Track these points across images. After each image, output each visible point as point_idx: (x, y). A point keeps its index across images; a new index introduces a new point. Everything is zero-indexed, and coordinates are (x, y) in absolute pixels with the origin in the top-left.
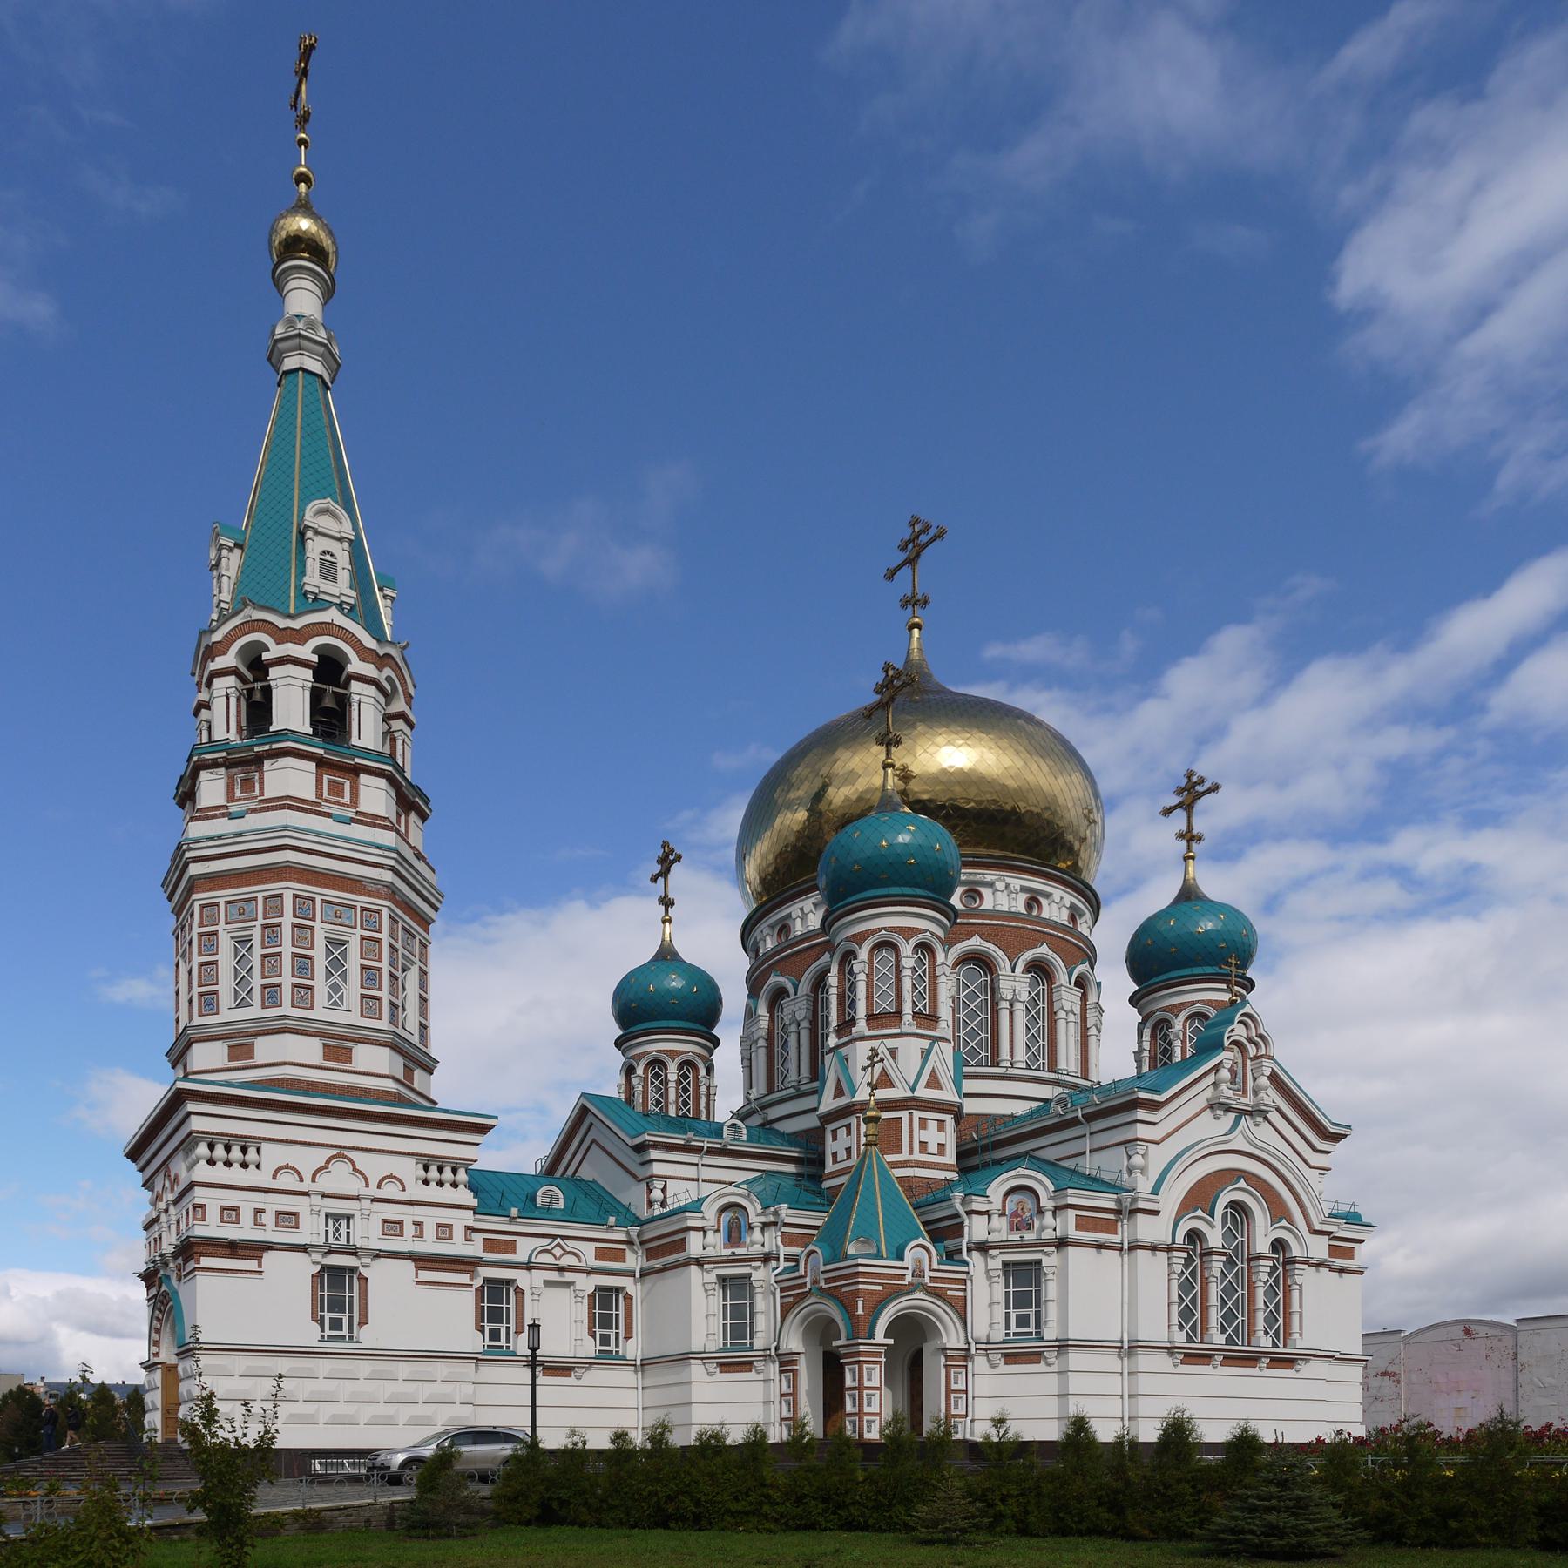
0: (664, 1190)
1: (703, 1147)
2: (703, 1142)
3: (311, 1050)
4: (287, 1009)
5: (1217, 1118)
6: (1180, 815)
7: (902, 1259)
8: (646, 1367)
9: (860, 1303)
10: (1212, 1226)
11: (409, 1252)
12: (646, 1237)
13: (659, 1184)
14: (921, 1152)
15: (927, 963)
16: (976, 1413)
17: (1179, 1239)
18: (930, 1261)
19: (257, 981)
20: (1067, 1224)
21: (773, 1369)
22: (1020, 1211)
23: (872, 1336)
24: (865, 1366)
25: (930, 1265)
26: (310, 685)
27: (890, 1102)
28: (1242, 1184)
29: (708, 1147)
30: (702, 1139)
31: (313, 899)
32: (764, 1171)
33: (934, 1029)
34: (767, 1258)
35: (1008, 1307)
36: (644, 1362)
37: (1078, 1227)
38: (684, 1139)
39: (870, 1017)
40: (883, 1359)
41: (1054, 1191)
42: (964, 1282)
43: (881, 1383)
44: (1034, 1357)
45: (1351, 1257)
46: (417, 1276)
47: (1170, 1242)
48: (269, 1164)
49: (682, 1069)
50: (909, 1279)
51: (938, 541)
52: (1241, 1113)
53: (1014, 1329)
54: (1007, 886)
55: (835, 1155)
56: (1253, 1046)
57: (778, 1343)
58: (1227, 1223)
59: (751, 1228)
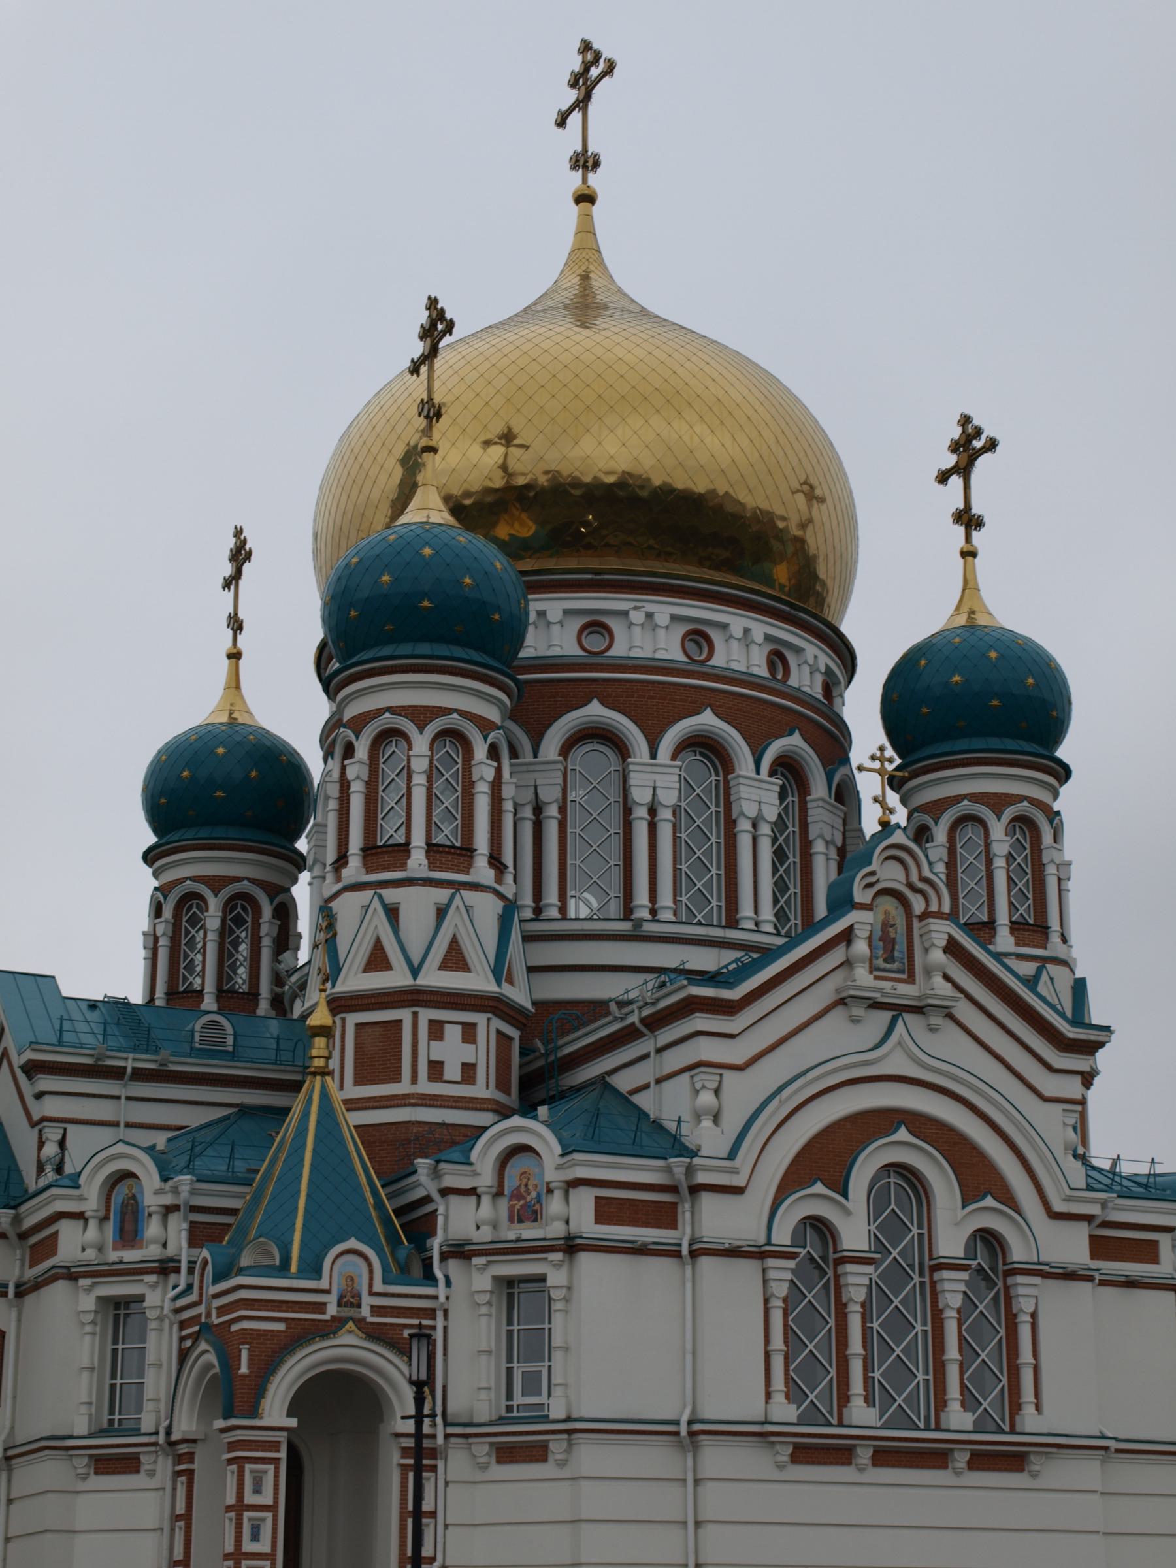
1: (125, 1068)
2: (126, 1059)
5: (855, 1021)
6: (956, 481)
8: (14, 1461)
9: (244, 1355)
10: (847, 1212)
12: (28, 1223)
13: (53, 1134)
17: (782, 1236)
18: (371, 1279)
20: (584, 1221)
21: (164, 1466)
22: (523, 1189)
23: (254, 1412)
24: (248, 1467)
25: (371, 1286)
28: (903, 1134)
29: (134, 1069)
30: (124, 1055)
33: (466, 870)
34: (166, 1268)
35: (510, 1359)
36: (10, 1453)
37: (600, 1218)
38: (92, 1056)
42: (431, 1313)
44: (536, 1453)
47: (762, 1240)
49: (234, 907)
50: (332, 1310)
51: (606, 79)
52: (899, 1009)
53: (519, 1399)
57: (171, 1421)
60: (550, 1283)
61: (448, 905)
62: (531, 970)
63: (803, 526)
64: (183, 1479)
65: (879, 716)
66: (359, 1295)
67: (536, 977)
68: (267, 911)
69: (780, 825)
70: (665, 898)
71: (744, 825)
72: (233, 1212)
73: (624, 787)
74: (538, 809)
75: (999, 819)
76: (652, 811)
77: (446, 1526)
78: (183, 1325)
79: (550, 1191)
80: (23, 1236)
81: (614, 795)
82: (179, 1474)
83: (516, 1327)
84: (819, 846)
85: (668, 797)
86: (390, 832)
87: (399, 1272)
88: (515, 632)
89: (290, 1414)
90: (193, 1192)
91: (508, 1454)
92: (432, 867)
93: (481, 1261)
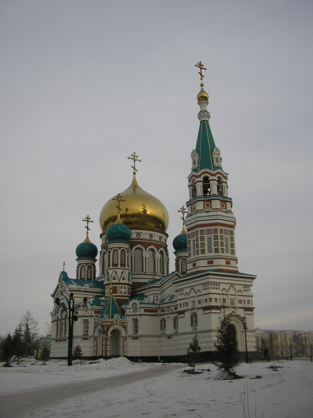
3: (223, 262)
4: (200, 255)
7: (113, 318)
9: (105, 328)
11: (243, 307)
14: (121, 293)
18: (119, 319)
19: (213, 247)
25: (119, 319)
26: (217, 184)
31: (222, 230)
35: (85, 329)
39: (113, 264)
40: (110, 339)
42: (126, 323)
43: (109, 344)
46: (245, 312)
48: (221, 288)
55: (106, 293)
59: (89, 310)
62: (132, 278)
63: (163, 219)
64: (96, 341)
65: (173, 246)
67: (132, 279)
69: (160, 260)
70: (147, 269)
71: (156, 260)
72: (101, 310)
74: (132, 258)
76: (146, 258)
77: (128, 347)
78: (95, 323)
79: (138, 308)
81: (141, 256)
82: (95, 340)
83: (135, 324)
84: (165, 262)
85: (148, 257)
86: (115, 262)
88: (130, 236)
90: (96, 307)
92: (121, 267)
93: (81, 317)
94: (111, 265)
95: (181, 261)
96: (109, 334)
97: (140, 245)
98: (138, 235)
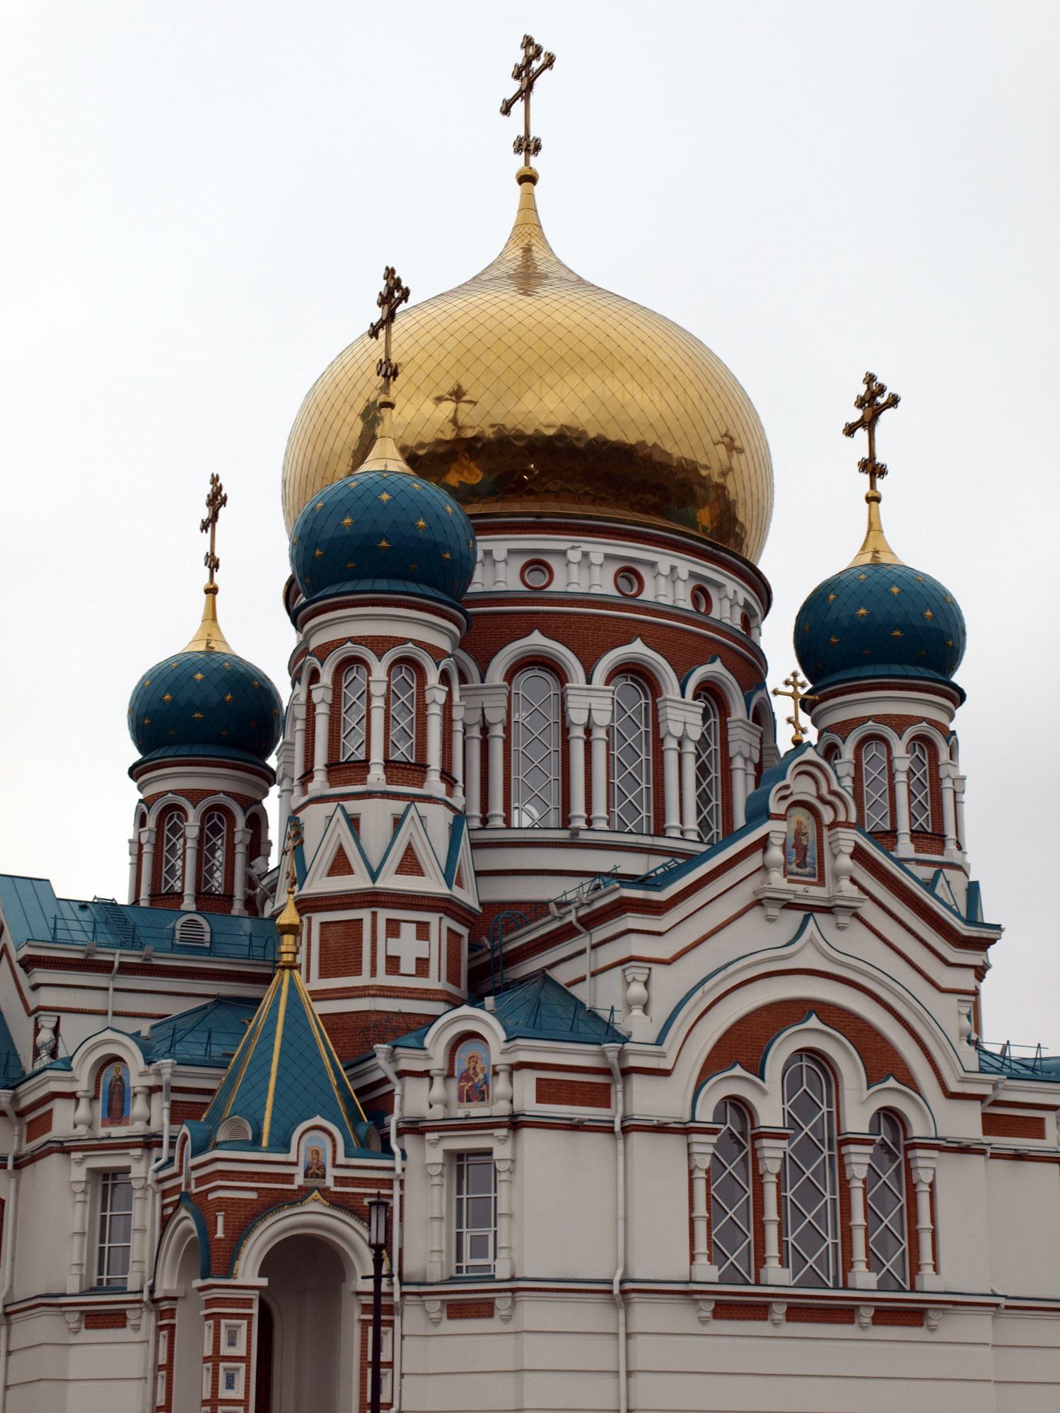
0: (56, 1031)
1: (113, 962)
2: (114, 954)
5: (771, 920)
6: (862, 434)
8: (13, 1317)
9: (220, 1221)
12: (26, 1102)
13: (48, 1022)
15: (414, 686)
16: (403, 1404)
17: (705, 1114)
18: (335, 1152)
20: (524, 1096)
21: (148, 1322)
22: (471, 1072)
23: (229, 1272)
24: (223, 1322)
25: (334, 1158)
27: (346, 896)
28: (814, 1022)
29: (121, 963)
32: (214, 996)
34: (150, 1142)
35: (459, 1225)
36: (9, 1309)
38: (83, 951)
40: (255, 1311)
41: (507, 1041)
42: (389, 1183)
43: (249, 1350)
44: (483, 1309)
45: (1041, 1135)
47: (687, 1117)
49: (212, 817)
50: (299, 1180)
53: (467, 1261)
54: (586, 555)
56: (828, 807)
58: (802, 1085)
60: (496, 1156)
61: (404, 816)
62: (479, 874)
64: (165, 1332)
65: (791, 645)
66: (324, 1167)
68: (241, 821)
69: (703, 743)
70: (600, 810)
71: (671, 744)
72: (210, 1092)
73: (563, 709)
74: (485, 729)
75: (900, 738)
76: (588, 731)
77: (402, 1375)
80: (21, 1114)
81: (553, 717)
84: (738, 763)
87: (360, 1146)
89: (261, 1275)
91: (457, 1310)
94: (320, 777)
95: (858, 757)
96: (248, 1271)
97: (545, 634)
98: (537, 574)
